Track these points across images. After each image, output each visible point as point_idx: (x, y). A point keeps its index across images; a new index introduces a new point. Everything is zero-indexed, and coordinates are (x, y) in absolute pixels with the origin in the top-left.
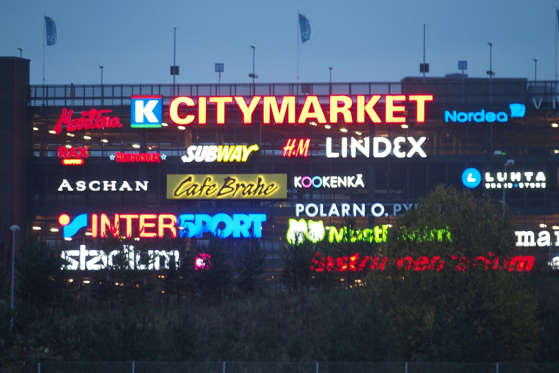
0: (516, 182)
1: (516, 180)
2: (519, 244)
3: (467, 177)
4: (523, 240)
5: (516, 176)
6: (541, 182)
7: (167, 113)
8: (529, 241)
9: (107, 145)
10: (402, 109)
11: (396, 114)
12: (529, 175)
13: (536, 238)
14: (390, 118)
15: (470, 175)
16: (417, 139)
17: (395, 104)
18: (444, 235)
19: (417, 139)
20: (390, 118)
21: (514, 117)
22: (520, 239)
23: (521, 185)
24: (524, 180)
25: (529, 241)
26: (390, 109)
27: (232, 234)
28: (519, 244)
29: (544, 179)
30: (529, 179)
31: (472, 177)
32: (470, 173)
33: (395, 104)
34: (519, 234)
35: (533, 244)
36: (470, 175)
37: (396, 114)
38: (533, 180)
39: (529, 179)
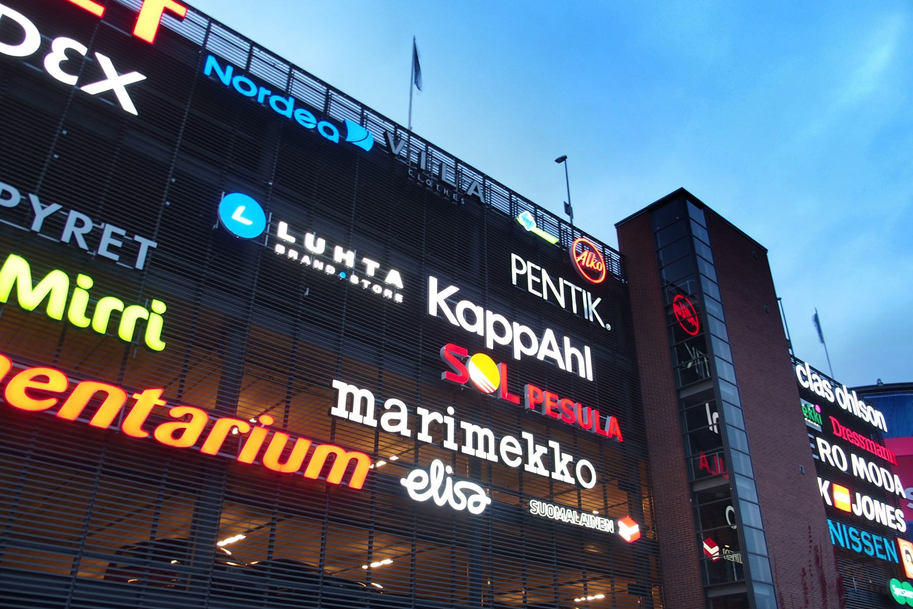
0: (341, 267)
1: (344, 261)
2: (339, 411)
3: (233, 210)
4: (349, 407)
5: (345, 256)
6: (392, 288)
7: (331, 489)
8: (364, 412)
9: (257, 418)
10: (119, 244)
11: (111, 248)
12: (372, 266)
13: (380, 411)
14: (103, 251)
15: (241, 209)
16: (131, 89)
17: (114, 235)
18: (141, 325)
19: (131, 89)
20: (103, 251)
21: (350, 143)
22: (342, 400)
23: (354, 279)
24: (360, 269)
25: (364, 412)
26: (106, 240)
27: (429, 413)
28: (339, 411)
29: (400, 285)
30: (370, 272)
31: (244, 215)
32: (243, 205)
33: (114, 235)
34: (342, 388)
35: (370, 420)
36: (241, 209)
37: (111, 248)
38: (379, 277)
39: (370, 272)
